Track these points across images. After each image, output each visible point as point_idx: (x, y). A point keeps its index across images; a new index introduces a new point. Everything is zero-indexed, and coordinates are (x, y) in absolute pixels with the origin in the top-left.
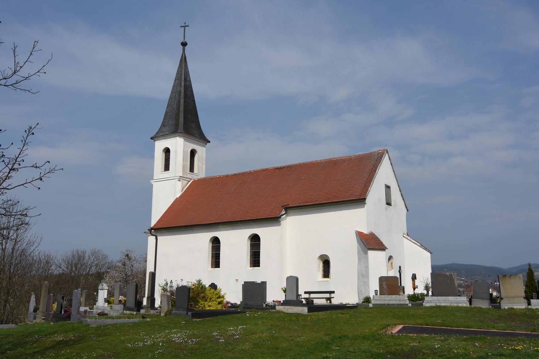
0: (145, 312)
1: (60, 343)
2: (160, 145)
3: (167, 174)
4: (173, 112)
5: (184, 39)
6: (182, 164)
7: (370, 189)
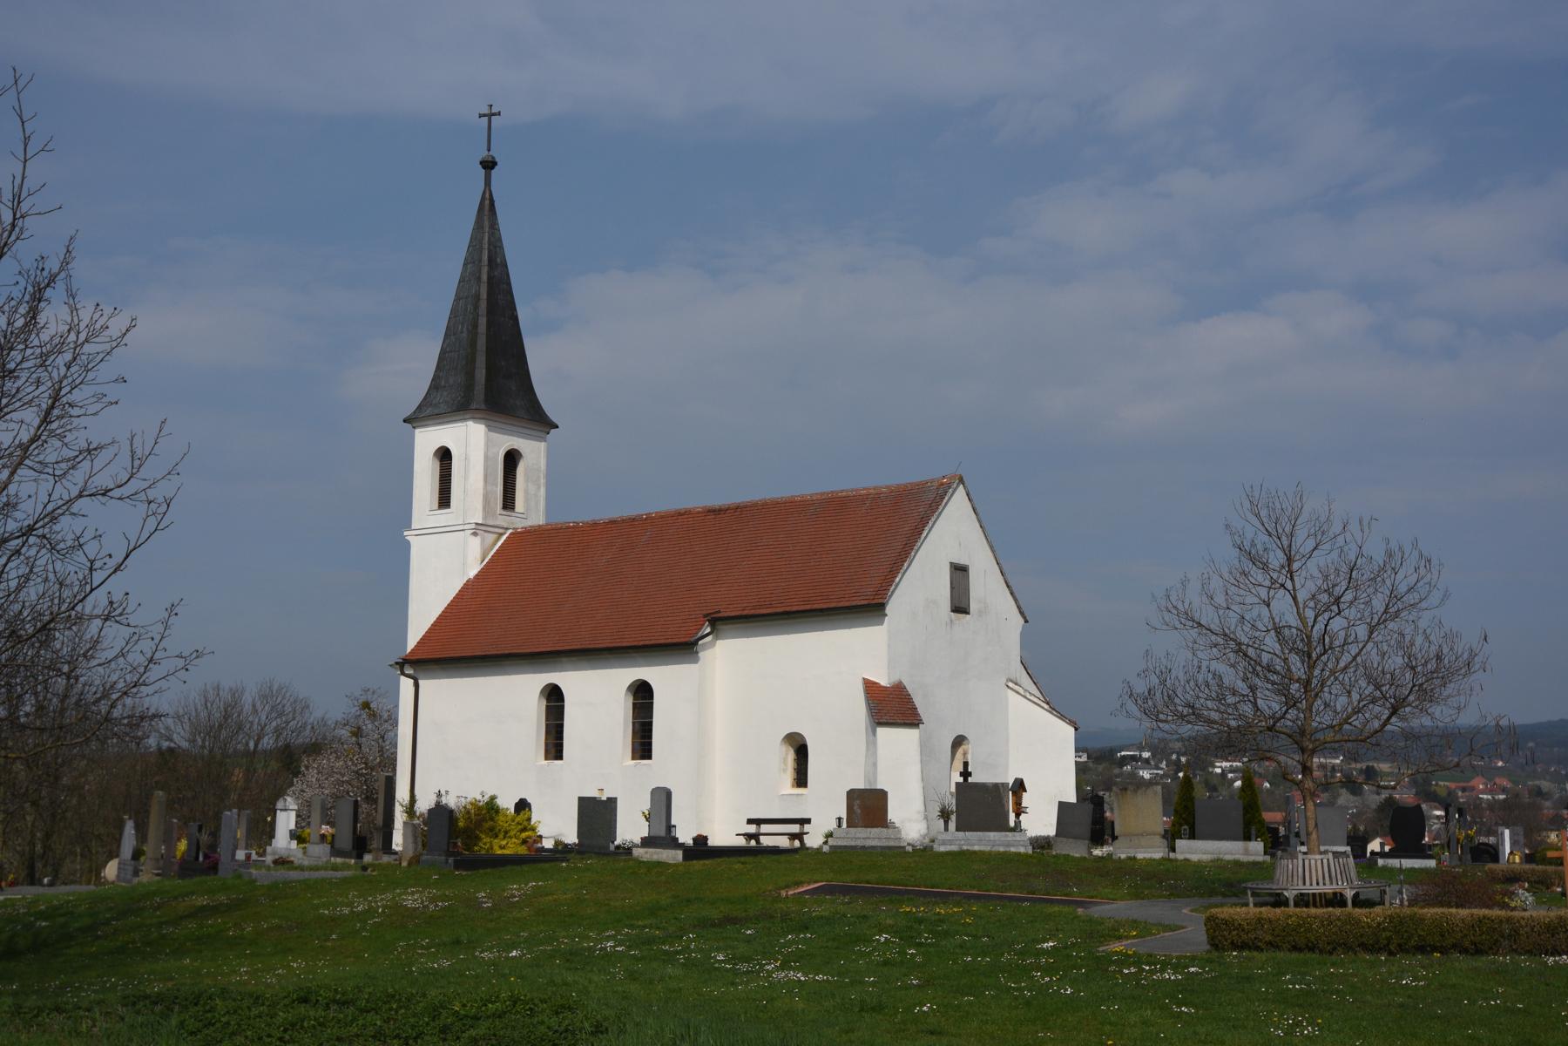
0: (373, 859)
1: (202, 909)
2: (428, 439)
3: (444, 517)
4: (459, 351)
5: (489, 150)
6: (481, 491)
7: (900, 580)
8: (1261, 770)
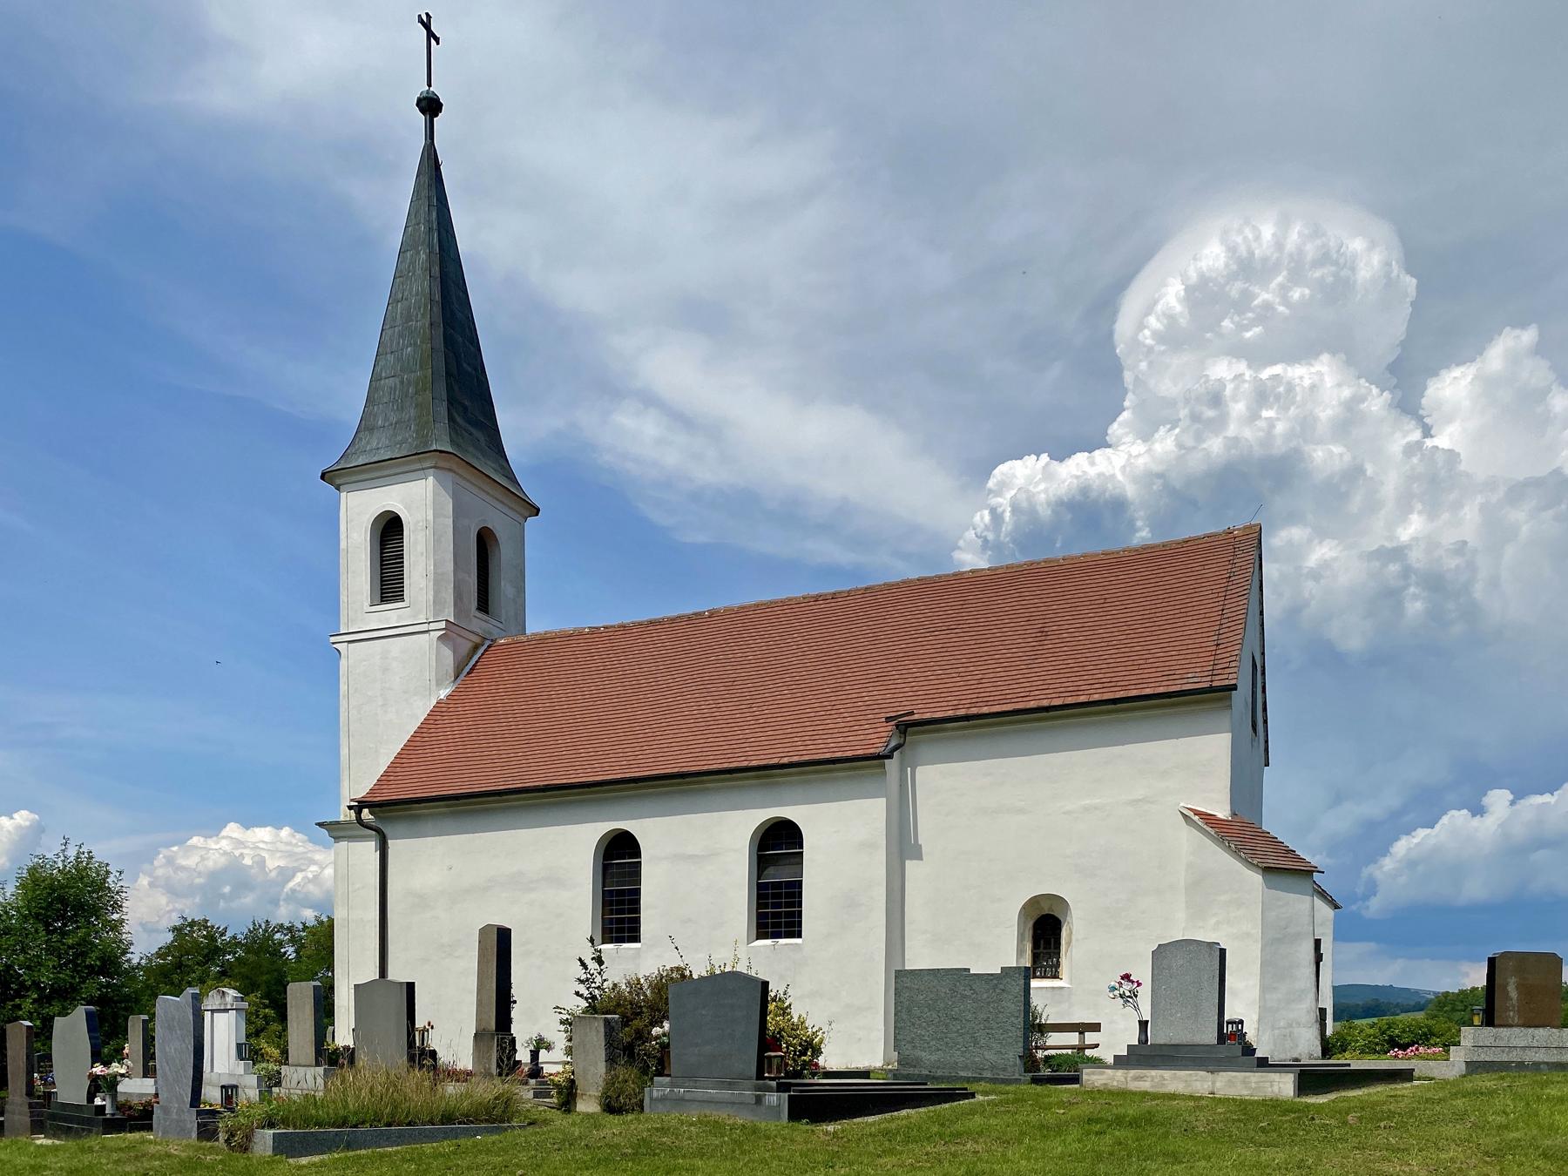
3: (391, 615)
8: (123, 1071)
